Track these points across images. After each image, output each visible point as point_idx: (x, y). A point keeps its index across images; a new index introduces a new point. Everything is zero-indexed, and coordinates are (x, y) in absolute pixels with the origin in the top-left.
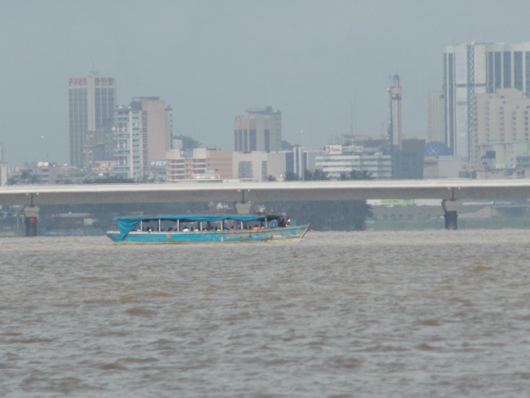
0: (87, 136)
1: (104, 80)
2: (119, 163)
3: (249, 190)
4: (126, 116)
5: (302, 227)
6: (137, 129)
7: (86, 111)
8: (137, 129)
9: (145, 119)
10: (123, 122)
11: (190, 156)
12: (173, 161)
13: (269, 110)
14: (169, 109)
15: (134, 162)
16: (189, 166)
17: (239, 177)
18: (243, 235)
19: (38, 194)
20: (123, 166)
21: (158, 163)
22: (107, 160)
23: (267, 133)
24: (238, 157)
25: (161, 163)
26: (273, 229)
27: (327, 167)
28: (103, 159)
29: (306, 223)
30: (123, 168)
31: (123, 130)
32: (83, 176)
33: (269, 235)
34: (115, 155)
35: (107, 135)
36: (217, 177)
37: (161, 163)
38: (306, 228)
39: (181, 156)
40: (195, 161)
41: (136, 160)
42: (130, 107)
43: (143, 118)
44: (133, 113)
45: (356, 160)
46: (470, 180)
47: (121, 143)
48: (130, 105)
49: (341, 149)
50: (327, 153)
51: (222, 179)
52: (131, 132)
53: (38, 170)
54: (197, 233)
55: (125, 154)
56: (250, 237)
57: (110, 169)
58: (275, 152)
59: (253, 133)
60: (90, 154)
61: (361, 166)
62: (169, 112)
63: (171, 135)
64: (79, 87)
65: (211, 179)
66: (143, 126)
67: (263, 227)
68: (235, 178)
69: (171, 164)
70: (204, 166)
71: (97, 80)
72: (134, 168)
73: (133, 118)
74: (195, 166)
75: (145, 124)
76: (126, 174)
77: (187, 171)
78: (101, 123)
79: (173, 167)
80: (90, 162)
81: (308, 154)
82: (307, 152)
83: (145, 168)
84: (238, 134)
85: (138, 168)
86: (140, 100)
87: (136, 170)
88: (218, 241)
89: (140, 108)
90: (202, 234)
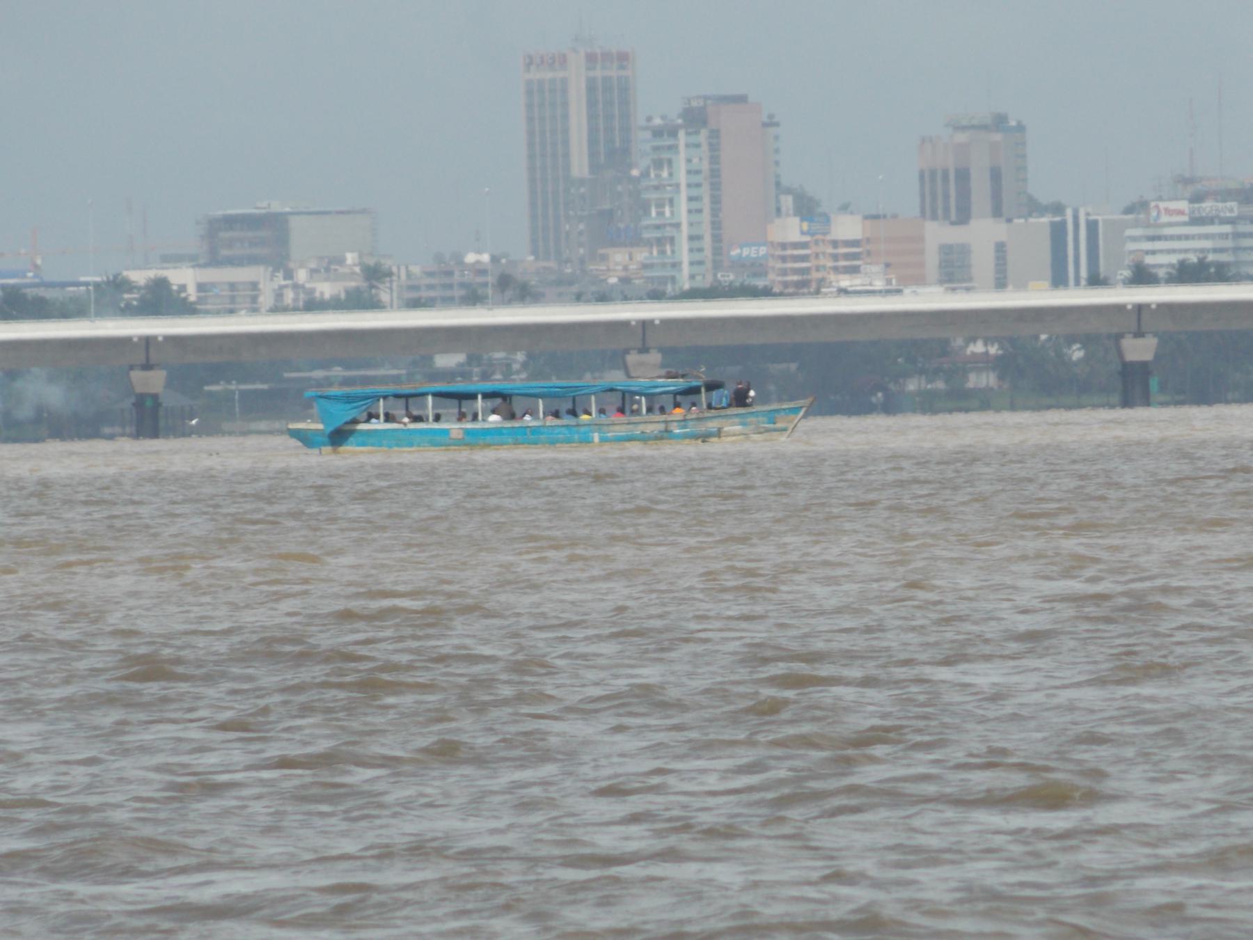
0: (573, 191)
1: (607, 56)
2: (655, 252)
3: (1153, 306)
4: (670, 142)
5: (792, 405)
6: (698, 172)
7: (566, 131)
8: (698, 172)
9: (714, 148)
10: (665, 155)
11: (825, 234)
12: (784, 246)
13: (1000, 122)
14: (771, 123)
15: (691, 250)
16: (821, 257)
17: (941, 282)
18: (649, 428)
19: (657, 322)
20: (666, 260)
21: (763, 250)
22: (625, 246)
23: (996, 175)
24: (937, 234)
25: (756, 252)
26: (723, 412)
27: (1153, 252)
28: (615, 243)
29: (805, 397)
30: (664, 265)
31: (665, 174)
32: (571, 283)
33: (712, 425)
34: (647, 235)
35: (619, 188)
36: (889, 282)
37: (756, 252)
38: (801, 407)
39: (803, 233)
40: (835, 244)
41: (696, 244)
42: (680, 121)
43: (710, 145)
44: (688, 134)
45: (1224, 236)
46: (490, 309)
47: (660, 205)
48: (680, 116)
49: (1187, 211)
50: (1152, 221)
51: (901, 287)
52: (682, 178)
53: (466, 272)
54: (530, 425)
55: (669, 232)
56: (666, 431)
57: (633, 267)
58: (1022, 221)
59: (963, 176)
60: (580, 233)
61: (1236, 250)
62: (772, 131)
63: (778, 184)
64: (549, 75)
65: (875, 286)
66: (711, 163)
67: (694, 408)
68: (930, 285)
69: (779, 252)
70: (855, 256)
71: (591, 58)
72: (692, 264)
73: (687, 146)
74: (835, 257)
75: (714, 160)
76: (673, 279)
77: (818, 269)
78: (602, 159)
79: (784, 259)
80: (581, 251)
81: (1101, 224)
82: (1099, 218)
83: (717, 266)
84: (930, 179)
85: (700, 263)
86: (702, 104)
87: (696, 269)
88: (587, 441)
89: (705, 123)
90: (544, 426)
